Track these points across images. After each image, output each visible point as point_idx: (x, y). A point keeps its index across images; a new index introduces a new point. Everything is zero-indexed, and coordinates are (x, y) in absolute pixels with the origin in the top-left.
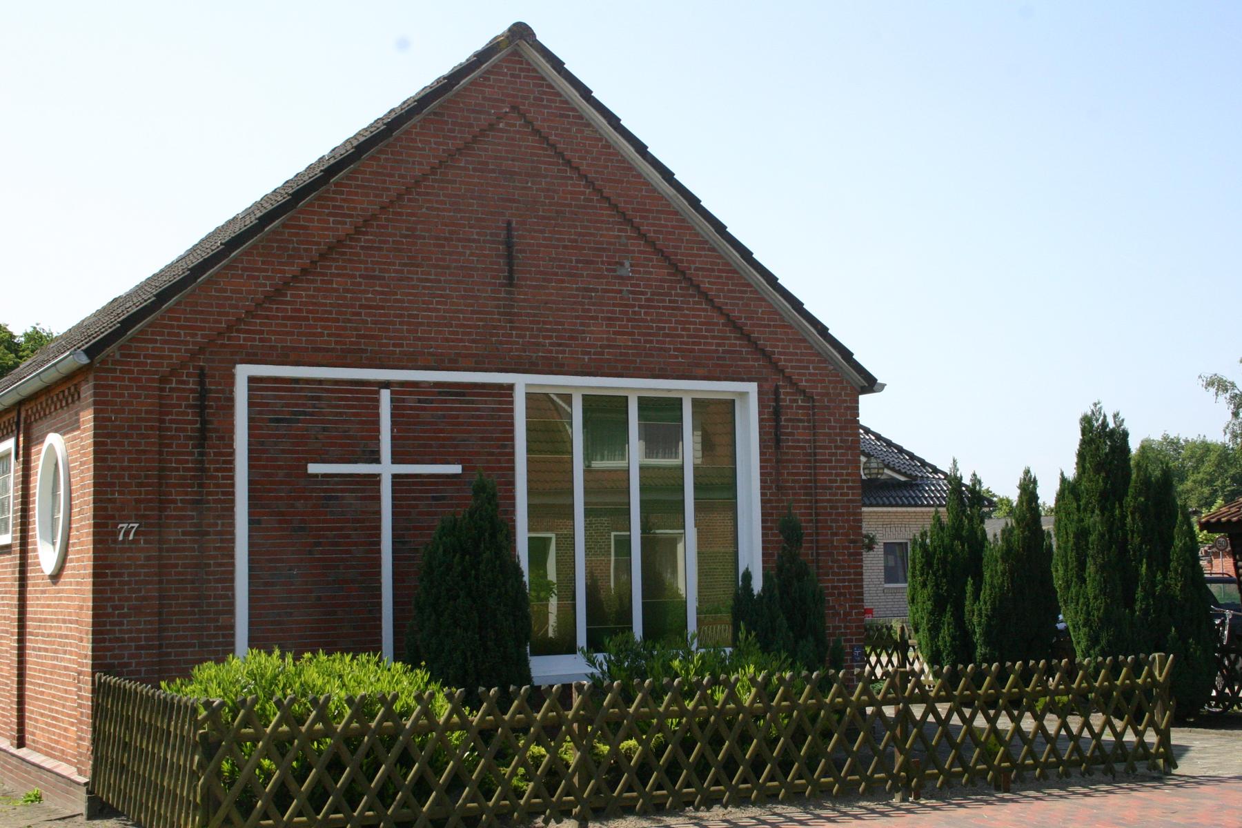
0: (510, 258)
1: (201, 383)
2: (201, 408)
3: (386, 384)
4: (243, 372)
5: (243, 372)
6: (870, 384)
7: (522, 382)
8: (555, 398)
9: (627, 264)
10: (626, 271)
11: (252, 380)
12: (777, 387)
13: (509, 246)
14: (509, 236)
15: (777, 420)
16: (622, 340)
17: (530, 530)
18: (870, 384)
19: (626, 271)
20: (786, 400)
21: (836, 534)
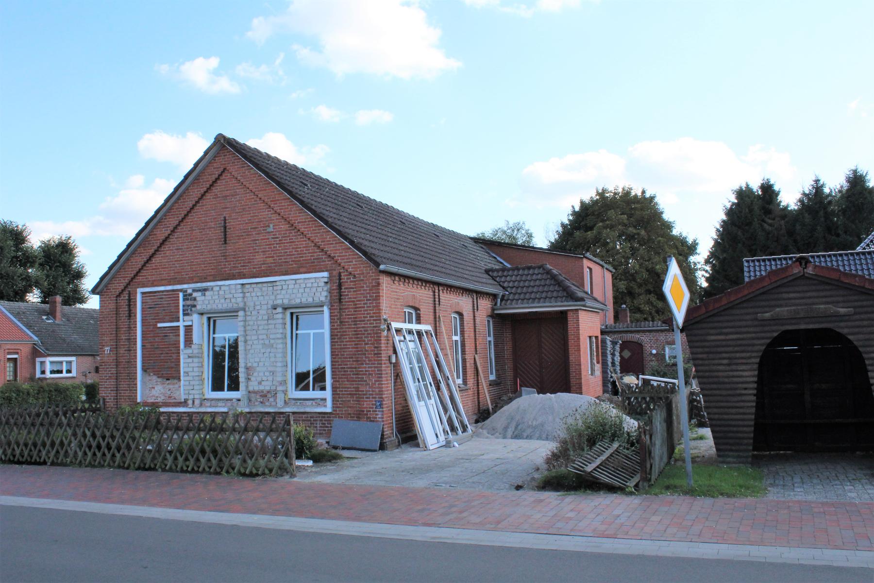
0: (225, 232)
1: (129, 296)
2: (129, 305)
3: (181, 290)
4: (139, 291)
5: (139, 291)
6: (818, 189)
7: (312, 332)
8: (306, 382)
9: (271, 226)
10: (271, 229)
11: (143, 293)
12: (340, 273)
13: (225, 227)
14: (225, 223)
15: (340, 289)
16: (270, 260)
17: (223, 390)
18: (818, 189)
19: (271, 229)
20: (344, 278)
21: (366, 344)
